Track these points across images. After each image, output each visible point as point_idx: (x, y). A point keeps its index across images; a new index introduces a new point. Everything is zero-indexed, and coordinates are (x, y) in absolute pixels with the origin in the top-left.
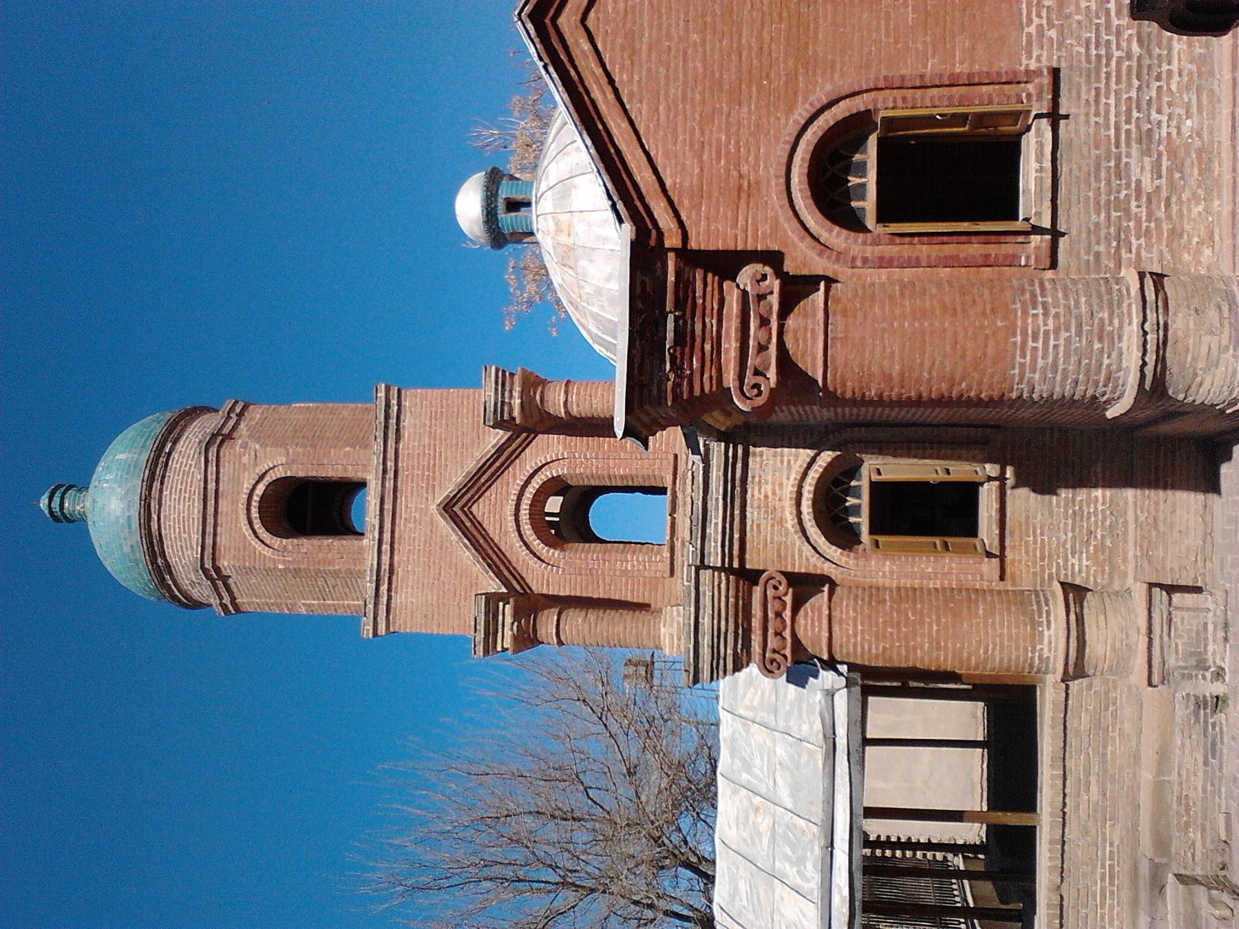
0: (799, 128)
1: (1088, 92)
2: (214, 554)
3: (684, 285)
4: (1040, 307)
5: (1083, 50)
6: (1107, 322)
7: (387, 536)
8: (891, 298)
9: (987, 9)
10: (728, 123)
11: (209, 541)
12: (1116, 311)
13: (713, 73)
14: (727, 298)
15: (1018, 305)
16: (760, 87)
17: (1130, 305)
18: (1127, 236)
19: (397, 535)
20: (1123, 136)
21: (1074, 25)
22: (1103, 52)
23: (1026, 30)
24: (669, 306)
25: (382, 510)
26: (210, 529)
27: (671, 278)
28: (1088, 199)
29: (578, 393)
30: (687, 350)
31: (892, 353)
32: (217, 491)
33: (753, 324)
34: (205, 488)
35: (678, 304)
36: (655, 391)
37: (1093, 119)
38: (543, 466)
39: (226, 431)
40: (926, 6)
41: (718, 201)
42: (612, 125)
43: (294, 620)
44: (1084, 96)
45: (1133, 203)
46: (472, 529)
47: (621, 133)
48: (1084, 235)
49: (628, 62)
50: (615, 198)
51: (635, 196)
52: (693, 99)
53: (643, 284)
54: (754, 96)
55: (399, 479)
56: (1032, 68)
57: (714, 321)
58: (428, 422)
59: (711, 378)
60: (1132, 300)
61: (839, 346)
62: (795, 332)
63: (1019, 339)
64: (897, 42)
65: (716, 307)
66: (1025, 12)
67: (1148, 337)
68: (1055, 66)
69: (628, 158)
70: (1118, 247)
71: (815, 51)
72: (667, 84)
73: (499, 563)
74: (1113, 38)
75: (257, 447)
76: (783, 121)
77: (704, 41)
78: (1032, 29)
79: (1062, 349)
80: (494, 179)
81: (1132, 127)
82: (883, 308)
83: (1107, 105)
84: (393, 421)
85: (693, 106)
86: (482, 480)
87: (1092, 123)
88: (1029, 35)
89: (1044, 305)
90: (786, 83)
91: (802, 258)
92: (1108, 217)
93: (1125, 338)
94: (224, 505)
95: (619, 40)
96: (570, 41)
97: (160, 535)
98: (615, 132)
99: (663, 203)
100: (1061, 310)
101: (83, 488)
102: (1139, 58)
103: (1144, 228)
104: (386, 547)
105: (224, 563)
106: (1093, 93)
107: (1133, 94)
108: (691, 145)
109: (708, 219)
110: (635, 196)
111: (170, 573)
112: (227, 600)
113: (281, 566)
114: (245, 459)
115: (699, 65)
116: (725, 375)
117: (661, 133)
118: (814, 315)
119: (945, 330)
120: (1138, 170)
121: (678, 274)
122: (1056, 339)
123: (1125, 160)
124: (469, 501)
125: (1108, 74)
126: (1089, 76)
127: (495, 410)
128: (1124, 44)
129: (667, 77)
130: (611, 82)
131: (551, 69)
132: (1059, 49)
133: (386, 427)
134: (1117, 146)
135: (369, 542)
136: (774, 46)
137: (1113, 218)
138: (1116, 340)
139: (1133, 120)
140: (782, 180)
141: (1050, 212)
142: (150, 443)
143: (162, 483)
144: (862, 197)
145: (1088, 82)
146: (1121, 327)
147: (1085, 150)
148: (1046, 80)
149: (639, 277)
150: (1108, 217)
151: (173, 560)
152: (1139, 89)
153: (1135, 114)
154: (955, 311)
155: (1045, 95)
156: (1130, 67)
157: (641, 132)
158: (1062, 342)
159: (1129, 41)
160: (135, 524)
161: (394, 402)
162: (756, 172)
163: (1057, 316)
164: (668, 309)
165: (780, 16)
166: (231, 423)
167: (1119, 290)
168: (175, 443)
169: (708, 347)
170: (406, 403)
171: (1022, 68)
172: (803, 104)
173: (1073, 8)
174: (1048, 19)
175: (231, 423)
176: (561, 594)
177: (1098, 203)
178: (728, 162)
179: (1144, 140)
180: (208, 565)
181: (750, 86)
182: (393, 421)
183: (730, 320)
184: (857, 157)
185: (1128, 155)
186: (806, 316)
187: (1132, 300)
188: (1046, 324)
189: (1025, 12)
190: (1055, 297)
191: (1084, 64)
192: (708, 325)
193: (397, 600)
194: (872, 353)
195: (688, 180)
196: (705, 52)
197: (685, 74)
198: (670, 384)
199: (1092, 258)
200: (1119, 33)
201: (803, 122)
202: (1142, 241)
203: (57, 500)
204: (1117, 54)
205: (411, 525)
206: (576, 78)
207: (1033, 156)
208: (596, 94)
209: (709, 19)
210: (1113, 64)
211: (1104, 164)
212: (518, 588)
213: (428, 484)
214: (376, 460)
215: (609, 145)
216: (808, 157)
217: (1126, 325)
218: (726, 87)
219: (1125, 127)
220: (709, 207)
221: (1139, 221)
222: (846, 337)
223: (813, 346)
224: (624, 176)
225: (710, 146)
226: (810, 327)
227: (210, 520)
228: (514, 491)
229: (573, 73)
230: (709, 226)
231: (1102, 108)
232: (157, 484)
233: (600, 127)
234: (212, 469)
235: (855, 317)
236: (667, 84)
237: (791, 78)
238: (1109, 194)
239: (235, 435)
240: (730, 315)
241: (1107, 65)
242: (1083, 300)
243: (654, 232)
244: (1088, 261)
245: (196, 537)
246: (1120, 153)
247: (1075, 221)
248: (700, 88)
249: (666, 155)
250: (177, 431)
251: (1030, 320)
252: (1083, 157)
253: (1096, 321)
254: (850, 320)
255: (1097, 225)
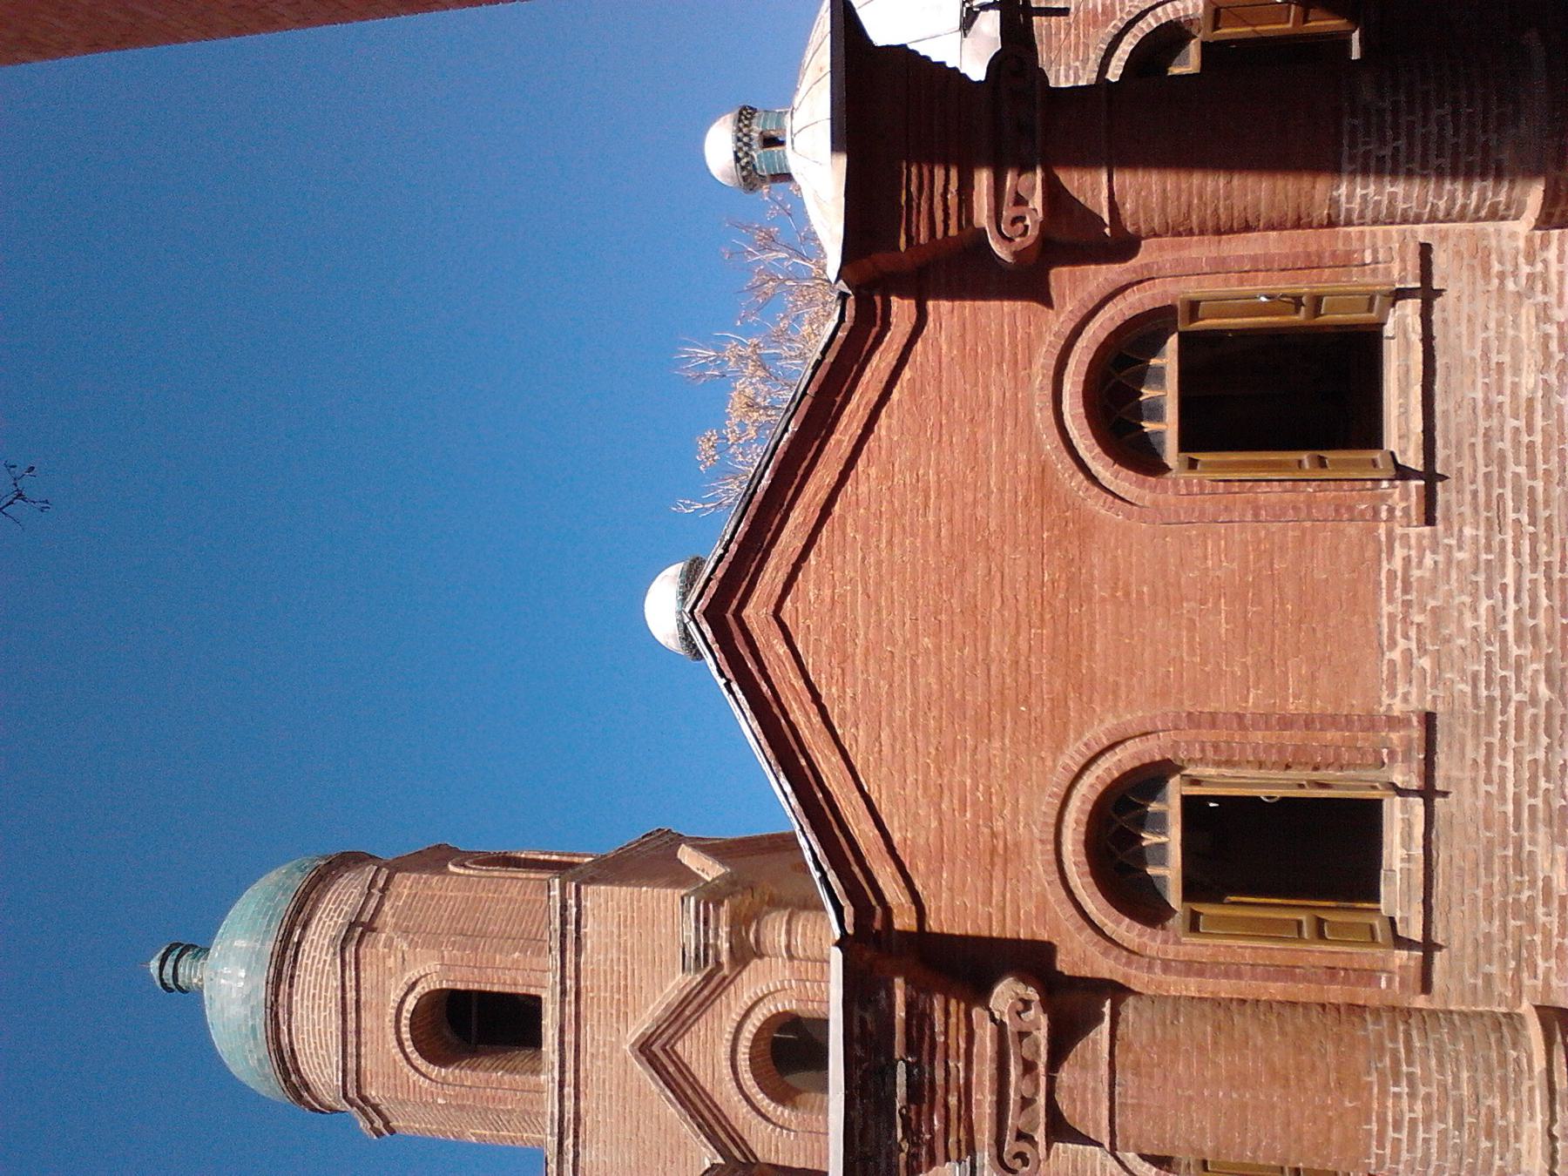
0: (1070, 776)
1: (1477, 747)
2: (358, 1080)
3: (918, 1017)
4: (1404, 1083)
5: (1468, 689)
6: (1498, 1113)
7: (570, 1076)
8: (1201, 1049)
9: (1332, 623)
10: (974, 761)
11: (352, 1064)
12: (1512, 1098)
13: (951, 690)
14: (978, 1031)
15: (1374, 1078)
16: (1016, 716)
17: (1531, 1089)
18: (1530, 955)
19: (582, 1075)
20: (1526, 815)
21: (1456, 652)
22: (1497, 693)
23: (1388, 655)
24: (899, 1050)
25: (562, 1043)
26: (351, 1049)
27: (900, 1013)
28: (1475, 899)
29: (804, 935)
30: (925, 1107)
31: (1202, 1129)
32: (358, 1001)
33: (1014, 1072)
34: (343, 998)
35: (911, 1048)
36: (883, 1166)
37: (1483, 788)
38: (765, 996)
39: (366, 918)
40: (1246, 612)
41: (964, 867)
42: (817, 757)
43: (459, 1147)
44: (1470, 754)
45: (1540, 910)
46: (677, 1076)
47: (831, 770)
48: (1469, 950)
49: (837, 671)
50: (825, 867)
51: (851, 859)
52: (926, 726)
53: (863, 1021)
54: (1008, 725)
55: (582, 1002)
56: (1396, 713)
57: (961, 1065)
58: (616, 931)
59: (959, 1141)
60: (1536, 1082)
61: (1129, 1113)
62: (1071, 1090)
63: (1375, 1127)
64: (1204, 662)
65: (963, 1045)
66: (1385, 630)
67: (1559, 1145)
68: (1429, 708)
69: (842, 804)
70: (1518, 970)
71: (1090, 668)
72: (891, 703)
73: (712, 1122)
74: (1511, 674)
75: (405, 947)
76: (1049, 763)
77: (938, 648)
78: (1396, 655)
79: (1434, 1144)
80: (745, 115)
81: (1539, 802)
82: (1189, 1066)
83: (1503, 769)
84: (571, 927)
85: (927, 736)
86: (687, 1013)
87: (1482, 793)
88: (1392, 662)
89: (1410, 1076)
90: (1052, 710)
91: (1079, 955)
92: (1504, 926)
93: (1525, 1138)
94: (368, 1020)
95: (826, 640)
96: (760, 642)
97: (292, 1050)
98: (823, 768)
99: (890, 868)
100: (1434, 1090)
101: (198, 949)
102: (1549, 705)
103: (1555, 945)
104: (569, 1090)
105: (372, 1093)
106: (1483, 751)
107: (1541, 755)
108: (925, 789)
109: (951, 889)
110: (851, 859)
111: (308, 1089)
112: (379, 1124)
113: (440, 1101)
114: (391, 962)
115: (932, 680)
116: (977, 1137)
117: (884, 770)
118: (1096, 1068)
119: (1273, 1107)
120: (1547, 865)
121: (910, 1005)
122: (1427, 1130)
123: (1527, 847)
124: (670, 1038)
125: (1504, 725)
126: (1476, 727)
127: (697, 956)
128: (1527, 684)
129: (890, 694)
130: (816, 698)
131: (735, 687)
132: (1434, 686)
133: (563, 935)
134: (1518, 826)
135: (548, 1078)
136: (1033, 659)
137: (1510, 929)
138: (1512, 1140)
139: (1541, 793)
140: (1050, 847)
141: (1421, 918)
142: (275, 925)
143: (291, 986)
144: (1162, 862)
145: (1476, 735)
146: (1518, 1122)
147: (1471, 830)
148: (1417, 733)
149: (857, 1012)
150: (1504, 926)
151: (311, 1078)
152: (1549, 748)
153: (1543, 784)
154: (1287, 1080)
155: (1414, 753)
156: (1535, 717)
157: (858, 768)
158: (1435, 1135)
159: (1534, 680)
160: (261, 1036)
161: (572, 902)
162: (1014, 830)
163: (1428, 1098)
164: (897, 1056)
165: (1042, 620)
166: (373, 903)
167: (1517, 1061)
168: (305, 928)
169: (953, 1101)
170: (587, 904)
171: (1382, 709)
172: (1076, 740)
173: (1453, 628)
174: (1419, 641)
175: (373, 903)
176: (795, 1165)
177: (1490, 905)
178: (975, 815)
179: (1556, 821)
180: (352, 1094)
181: (1002, 712)
182: (571, 927)
183: (982, 1063)
184: (1153, 807)
185: (1533, 842)
186: (1084, 1068)
187: (1536, 1082)
188: (1411, 1110)
189: (1385, 630)
190: (1425, 1067)
191: (1470, 709)
192: (953, 1071)
193: (586, 1157)
194: (1175, 1126)
195: (923, 833)
196: (940, 664)
197: (915, 691)
198: (903, 1156)
199: (1480, 982)
200: (1519, 668)
201: (1076, 769)
202: (1553, 962)
203: (168, 969)
204: (1516, 697)
205: (600, 1063)
206: (769, 694)
207: (1397, 839)
208: (797, 716)
209: (944, 617)
210: (1512, 710)
211: (1498, 852)
212: (737, 1154)
213: (618, 1011)
214: (552, 978)
215: (816, 788)
216: (1085, 818)
217: (1525, 1119)
218: (970, 713)
219: (1527, 801)
220: (952, 874)
221: (1547, 935)
222: (1140, 1105)
223: (1094, 1113)
224: (837, 832)
225: (951, 791)
226: (1091, 1085)
227: (352, 1038)
228: (729, 1028)
229: (764, 687)
230: (953, 899)
231: (1495, 773)
232: (284, 987)
233: (803, 763)
234: (351, 973)
235: (1151, 1077)
236: (891, 703)
237: (1059, 704)
238: (1505, 894)
239: (378, 923)
240: (981, 1056)
241: (1504, 712)
242: (1465, 1075)
243: (879, 910)
244: (1475, 986)
245: (336, 1059)
246: (1521, 838)
247: (1456, 929)
248: (935, 712)
249: (892, 801)
250: (307, 910)
251: (1390, 1103)
252: (1468, 839)
253: (1483, 1112)
254: (1145, 1080)
255: (1488, 936)
